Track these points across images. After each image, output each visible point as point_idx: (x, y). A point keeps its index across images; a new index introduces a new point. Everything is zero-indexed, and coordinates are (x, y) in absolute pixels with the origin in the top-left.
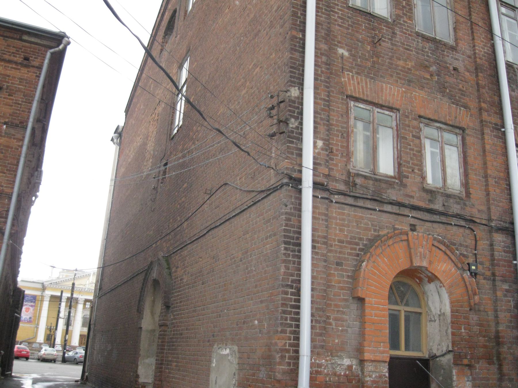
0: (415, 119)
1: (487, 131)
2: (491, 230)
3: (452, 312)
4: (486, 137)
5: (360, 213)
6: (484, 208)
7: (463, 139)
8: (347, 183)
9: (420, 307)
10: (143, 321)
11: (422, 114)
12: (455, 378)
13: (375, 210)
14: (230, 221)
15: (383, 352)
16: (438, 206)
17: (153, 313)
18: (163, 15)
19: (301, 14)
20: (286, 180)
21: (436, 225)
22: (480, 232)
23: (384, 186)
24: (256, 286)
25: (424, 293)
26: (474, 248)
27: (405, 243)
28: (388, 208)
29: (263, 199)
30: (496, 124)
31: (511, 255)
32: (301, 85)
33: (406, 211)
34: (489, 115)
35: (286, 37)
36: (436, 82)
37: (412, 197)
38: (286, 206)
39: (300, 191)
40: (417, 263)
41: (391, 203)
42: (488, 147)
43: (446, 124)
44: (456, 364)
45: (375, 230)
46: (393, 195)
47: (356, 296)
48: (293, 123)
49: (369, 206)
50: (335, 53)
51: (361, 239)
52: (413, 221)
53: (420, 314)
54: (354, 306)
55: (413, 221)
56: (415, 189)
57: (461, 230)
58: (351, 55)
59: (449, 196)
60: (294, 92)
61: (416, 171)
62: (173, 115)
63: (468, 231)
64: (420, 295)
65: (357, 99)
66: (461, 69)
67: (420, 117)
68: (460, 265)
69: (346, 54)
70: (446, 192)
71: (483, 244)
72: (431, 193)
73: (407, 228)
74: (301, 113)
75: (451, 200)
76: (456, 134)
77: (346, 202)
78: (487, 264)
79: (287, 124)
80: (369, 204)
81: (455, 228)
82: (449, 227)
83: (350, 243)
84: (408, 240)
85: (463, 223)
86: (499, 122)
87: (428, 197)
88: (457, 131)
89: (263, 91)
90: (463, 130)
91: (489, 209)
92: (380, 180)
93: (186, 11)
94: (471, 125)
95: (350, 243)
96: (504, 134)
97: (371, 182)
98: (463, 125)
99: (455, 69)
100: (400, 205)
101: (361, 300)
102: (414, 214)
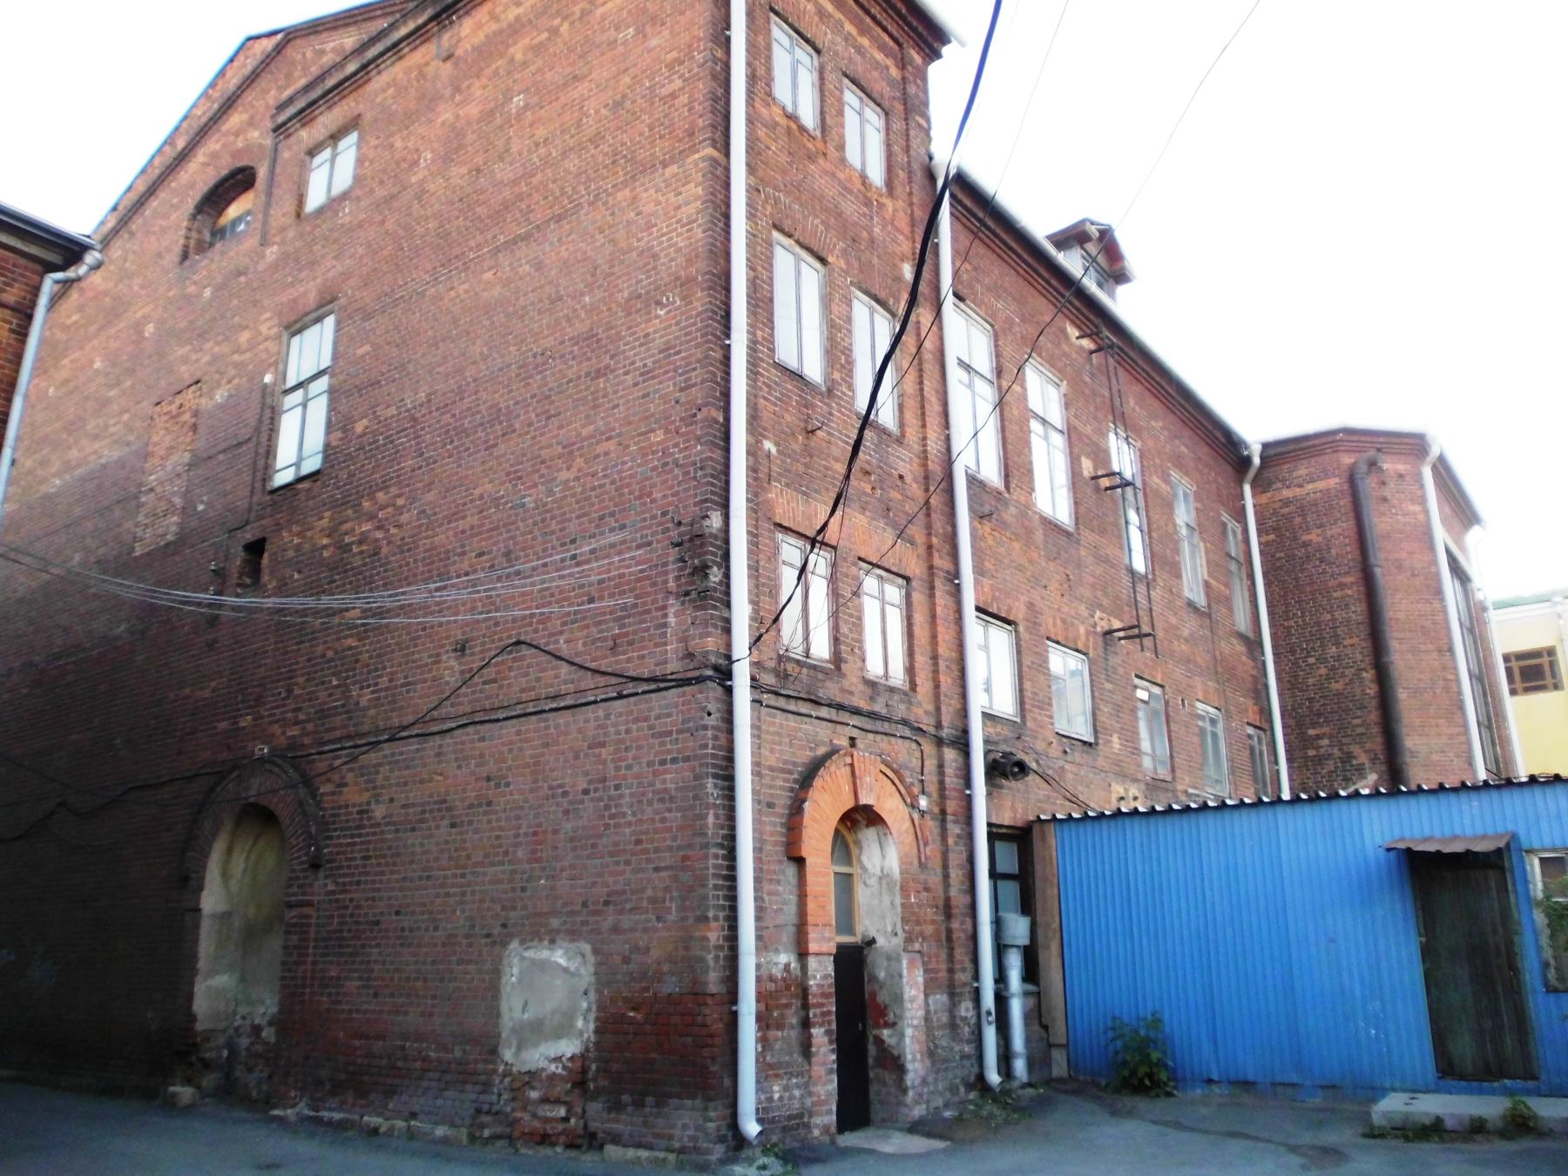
0: (855, 564)
1: (938, 583)
2: (939, 742)
3: (901, 873)
4: (938, 594)
5: (792, 721)
6: (930, 707)
7: (908, 596)
8: (777, 675)
9: (849, 863)
10: (205, 894)
11: (863, 556)
12: (905, 972)
13: (810, 716)
14: (544, 716)
15: (830, 940)
16: (879, 707)
17: (225, 875)
18: (182, 157)
19: (722, 378)
20: (709, 673)
21: (879, 737)
22: (929, 748)
23: (820, 676)
24: (638, 842)
25: (858, 843)
26: (919, 770)
27: (848, 769)
28: (824, 712)
29: (644, 692)
30: (948, 572)
31: (962, 781)
32: (725, 506)
33: (844, 717)
34: (941, 558)
35: (695, 415)
36: (879, 500)
37: (851, 693)
38: (709, 714)
39: (729, 691)
40: (864, 801)
41: (829, 706)
42: (939, 610)
43: (888, 571)
44: (905, 950)
45: (811, 749)
46: (830, 690)
47: (795, 855)
48: (715, 576)
49: (803, 711)
50: (761, 449)
51: (795, 764)
52: (855, 733)
53: (851, 875)
54: (791, 870)
55: (855, 733)
56: (854, 680)
57: (907, 743)
58: (778, 451)
59: (892, 690)
60: (716, 521)
61: (856, 651)
62: (270, 436)
63: (914, 745)
64: (852, 846)
65: (787, 530)
66: (908, 479)
67: (860, 559)
68: (909, 800)
69: (774, 450)
70: (888, 683)
71: (931, 764)
72: (872, 684)
73: (845, 743)
74: (726, 556)
75: (896, 697)
76: (900, 587)
77: (778, 705)
78: (935, 795)
79: (706, 576)
80: (804, 708)
81: (900, 741)
82: (893, 740)
83: (782, 771)
84: (852, 765)
85: (907, 733)
86: (950, 567)
87: (869, 691)
88: (900, 581)
89: (630, 493)
90: (907, 579)
91: (938, 709)
92: (814, 667)
93: (301, 200)
94: (918, 571)
95: (782, 771)
96: (958, 587)
97: (805, 671)
98: (908, 573)
99: (901, 477)
100: (840, 707)
101: (800, 861)
102: (855, 720)
